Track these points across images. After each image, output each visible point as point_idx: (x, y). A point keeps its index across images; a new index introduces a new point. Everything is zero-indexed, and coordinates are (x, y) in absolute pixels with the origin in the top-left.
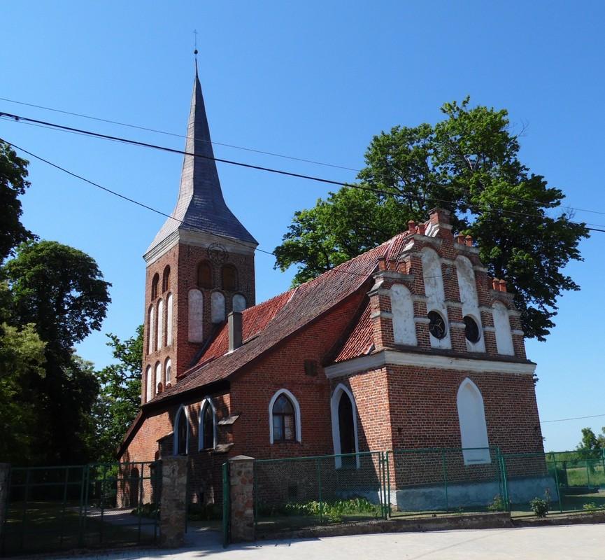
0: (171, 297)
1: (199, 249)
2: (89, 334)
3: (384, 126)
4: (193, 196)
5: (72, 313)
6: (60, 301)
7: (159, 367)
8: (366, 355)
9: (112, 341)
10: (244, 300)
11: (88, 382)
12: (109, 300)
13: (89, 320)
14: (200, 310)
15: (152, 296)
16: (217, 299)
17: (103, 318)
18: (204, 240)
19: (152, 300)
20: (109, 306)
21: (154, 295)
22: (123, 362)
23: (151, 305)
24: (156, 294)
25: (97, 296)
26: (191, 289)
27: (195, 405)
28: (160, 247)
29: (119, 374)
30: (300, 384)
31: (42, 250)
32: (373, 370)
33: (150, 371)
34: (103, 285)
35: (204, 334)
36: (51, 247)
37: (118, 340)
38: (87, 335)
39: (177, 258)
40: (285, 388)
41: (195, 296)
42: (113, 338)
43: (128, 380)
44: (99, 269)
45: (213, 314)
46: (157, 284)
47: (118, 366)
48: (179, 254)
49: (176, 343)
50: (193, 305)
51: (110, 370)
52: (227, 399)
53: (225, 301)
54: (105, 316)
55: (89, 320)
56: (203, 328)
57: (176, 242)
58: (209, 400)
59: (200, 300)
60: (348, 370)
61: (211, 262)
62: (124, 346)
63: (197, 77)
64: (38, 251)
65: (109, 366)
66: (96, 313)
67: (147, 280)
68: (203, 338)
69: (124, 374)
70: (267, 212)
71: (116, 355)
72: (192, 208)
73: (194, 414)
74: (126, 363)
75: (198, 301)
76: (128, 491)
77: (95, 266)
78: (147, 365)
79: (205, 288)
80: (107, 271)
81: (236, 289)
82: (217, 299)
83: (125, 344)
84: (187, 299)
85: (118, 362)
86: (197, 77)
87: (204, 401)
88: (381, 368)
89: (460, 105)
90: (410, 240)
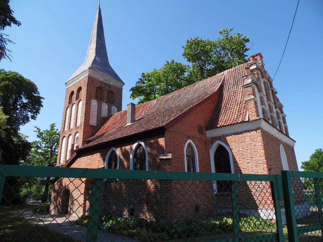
0: (81, 103)
1: (98, 81)
2: (29, 122)
3: (193, 37)
4: (95, 57)
5: (21, 110)
6: (16, 101)
7: (71, 137)
8: (246, 121)
9: (36, 130)
10: (117, 109)
11: (27, 146)
12: (42, 106)
13: (30, 114)
14: (96, 110)
15: (69, 102)
16: (104, 106)
17: (38, 114)
18: (101, 77)
19: (69, 104)
20: (41, 108)
21: (70, 102)
22: (41, 140)
23: (68, 107)
24: (71, 101)
25: (36, 104)
26: (92, 99)
27: (128, 148)
28: (76, 78)
29: (39, 145)
30: (197, 138)
31: (8, 75)
32: (248, 131)
33: (65, 139)
34: (39, 98)
35: (97, 122)
36: (14, 74)
37: (40, 130)
38: (28, 122)
39: (86, 83)
40: (191, 139)
41: (94, 103)
42: (38, 129)
43: (43, 148)
44: (38, 90)
45: (102, 113)
46: (72, 97)
47: (39, 142)
48: (88, 81)
49: (83, 124)
50: (93, 107)
51: (35, 143)
52: (162, 141)
53: (108, 108)
54: (39, 113)
55: (30, 114)
56: (97, 119)
57: (87, 75)
58: (142, 144)
59: (96, 105)
60: (225, 132)
61: (102, 89)
62: (42, 133)
63: (99, 6)
64: (6, 75)
65: (35, 141)
66: (34, 111)
67: (66, 96)
68: (97, 124)
69: (41, 145)
70: (129, 73)
71: (38, 136)
72: (94, 62)
73: (126, 154)
74: (43, 140)
75: (95, 105)
76: (59, 203)
77: (37, 89)
78: (63, 136)
79: (99, 100)
80: (42, 91)
81: (114, 103)
82: (104, 106)
83: (43, 132)
84: (90, 103)
85: (39, 140)
86: (99, 6)
87: (136, 144)
88: (256, 130)
89: (229, 30)
90: (253, 64)
